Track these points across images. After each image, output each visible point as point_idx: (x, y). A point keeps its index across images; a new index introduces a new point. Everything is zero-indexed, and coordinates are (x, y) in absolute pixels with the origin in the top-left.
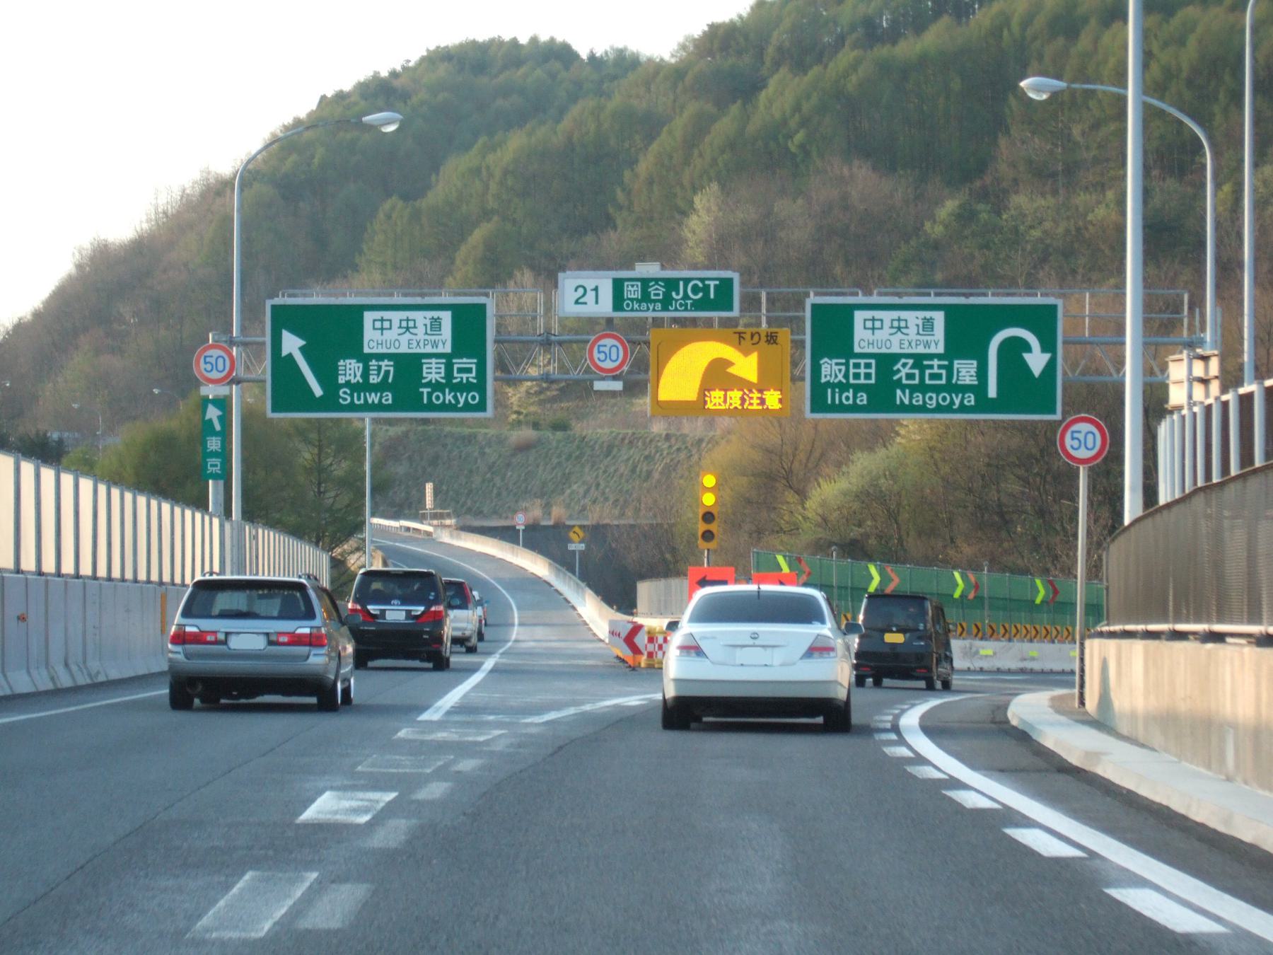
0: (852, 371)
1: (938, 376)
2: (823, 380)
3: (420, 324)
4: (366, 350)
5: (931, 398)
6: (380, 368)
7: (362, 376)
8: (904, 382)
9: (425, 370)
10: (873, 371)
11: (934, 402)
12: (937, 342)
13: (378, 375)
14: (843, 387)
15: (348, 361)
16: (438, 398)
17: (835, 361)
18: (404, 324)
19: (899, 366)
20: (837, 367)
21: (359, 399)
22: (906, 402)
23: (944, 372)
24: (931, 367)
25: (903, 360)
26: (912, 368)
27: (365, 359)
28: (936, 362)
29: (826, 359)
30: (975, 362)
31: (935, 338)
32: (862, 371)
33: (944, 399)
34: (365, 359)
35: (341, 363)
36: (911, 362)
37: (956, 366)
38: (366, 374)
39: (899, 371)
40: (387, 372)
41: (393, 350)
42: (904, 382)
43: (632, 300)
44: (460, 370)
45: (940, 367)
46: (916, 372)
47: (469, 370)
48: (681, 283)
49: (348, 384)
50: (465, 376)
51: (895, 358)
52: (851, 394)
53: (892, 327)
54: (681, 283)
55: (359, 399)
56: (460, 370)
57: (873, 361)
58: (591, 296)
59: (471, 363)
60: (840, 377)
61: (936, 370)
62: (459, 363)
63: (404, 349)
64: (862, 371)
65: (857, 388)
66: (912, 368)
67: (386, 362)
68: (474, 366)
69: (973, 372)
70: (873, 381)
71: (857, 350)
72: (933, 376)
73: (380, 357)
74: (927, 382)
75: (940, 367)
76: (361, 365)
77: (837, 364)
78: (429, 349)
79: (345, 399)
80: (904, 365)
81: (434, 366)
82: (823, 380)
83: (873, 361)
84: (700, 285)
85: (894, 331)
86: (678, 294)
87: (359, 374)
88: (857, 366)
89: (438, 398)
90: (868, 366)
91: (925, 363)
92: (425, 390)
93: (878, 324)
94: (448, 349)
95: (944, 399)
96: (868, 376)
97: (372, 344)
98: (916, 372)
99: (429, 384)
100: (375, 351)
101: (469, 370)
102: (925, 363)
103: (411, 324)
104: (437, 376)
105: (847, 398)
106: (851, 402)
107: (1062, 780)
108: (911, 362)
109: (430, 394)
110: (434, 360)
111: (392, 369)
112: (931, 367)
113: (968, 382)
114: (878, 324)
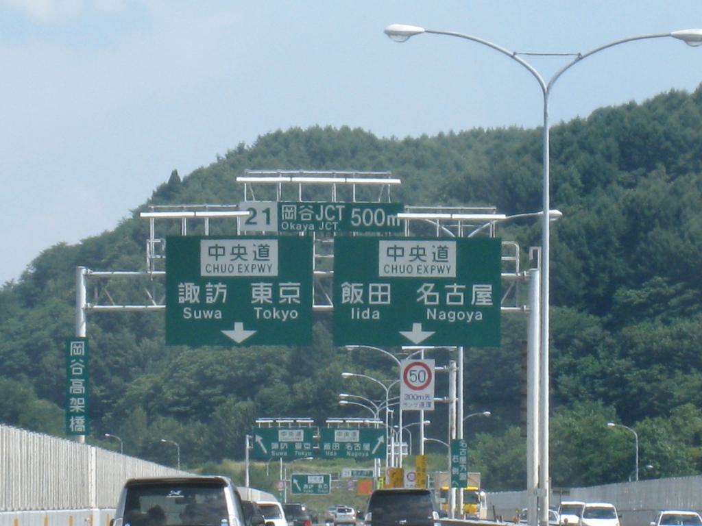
0: (371, 293)
1: (457, 299)
2: (344, 301)
3: (429, 252)
4: (203, 273)
5: (452, 315)
6: (215, 290)
7: (362, 298)
8: (426, 303)
9: (254, 293)
10: (389, 293)
11: (454, 317)
12: (450, 268)
13: (213, 296)
14: (363, 307)
15: (187, 284)
16: (267, 314)
17: (353, 285)
18: (415, 252)
19: (422, 289)
20: (356, 290)
21: (198, 315)
22: (434, 318)
23: (462, 294)
24: (452, 290)
25: (426, 285)
26: (433, 291)
27: (202, 282)
28: (455, 286)
29: (346, 283)
30: (490, 287)
31: (448, 264)
32: (380, 294)
33: (461, 316)
34: (202, 282)
35: (181, 285)
36: (432, 286)
37: (474, 290)
38: (202, 296)
39: (421, 294)
40: (221, 295)
41: (227, 274)
42: (426, 303)
43: (289, 221)
44: (285, 293)
45: (459, 290)
46: (437, 294)
47: (294, 292)
48: (322, 207)
49: (187, 304)
50: (290, 297)
51: (419, 282)
52: (368, 312)
53: (233, 254)
54: (322, 207)
55: (198, 315)
56: (285, 293)
57: (388, 286)
58: (261, 217)
59: (295, 286)
60: (359, 299)
61: (455, 293)
62: (283, 286)
63: (236, 273)
64: (380, 294)
65: (373, 308)
66: (433, 291)
67: (220, 285)
68: (298, 289)
69: (489, 294)
70: (389, 302)
71: (382, 274)
72: (452, 298)
73: (215, 280)
74: (448, 302)
75: (459, 290)
76: (198, 288)
77: (356, 287)
78: (256, 273)
79: (187, 315)
80: (426, 289)
81: (262, 289)
82: (344, 301)
83: (388, 286)
84: (333, 208)
85: (235, 257)
86: (319, 216)
87: (196, 296)
88: (384, 289)
89: (267, 314)
90: (384, 289)
91: (447, 286)
92: (258, 309)
93: (220, 251)
94: (274, 272)
95: (461, 316)
96: (384, 298)
97: (209, 268)
98: (437, 294)
99: (258, 304)
100: (212, 274)
101: (294, 292)
102: (447, 286)
103: (421, 252)
104: (265, 298)
105: (366, 315)
106: (368, 317)
107: (541, 484)
108: (432, 286)
109: (261, 312)
110: (262, 284)
111: (225, 291)
112: (452, 290)
113: (484, 304)
114: (399, 252)
